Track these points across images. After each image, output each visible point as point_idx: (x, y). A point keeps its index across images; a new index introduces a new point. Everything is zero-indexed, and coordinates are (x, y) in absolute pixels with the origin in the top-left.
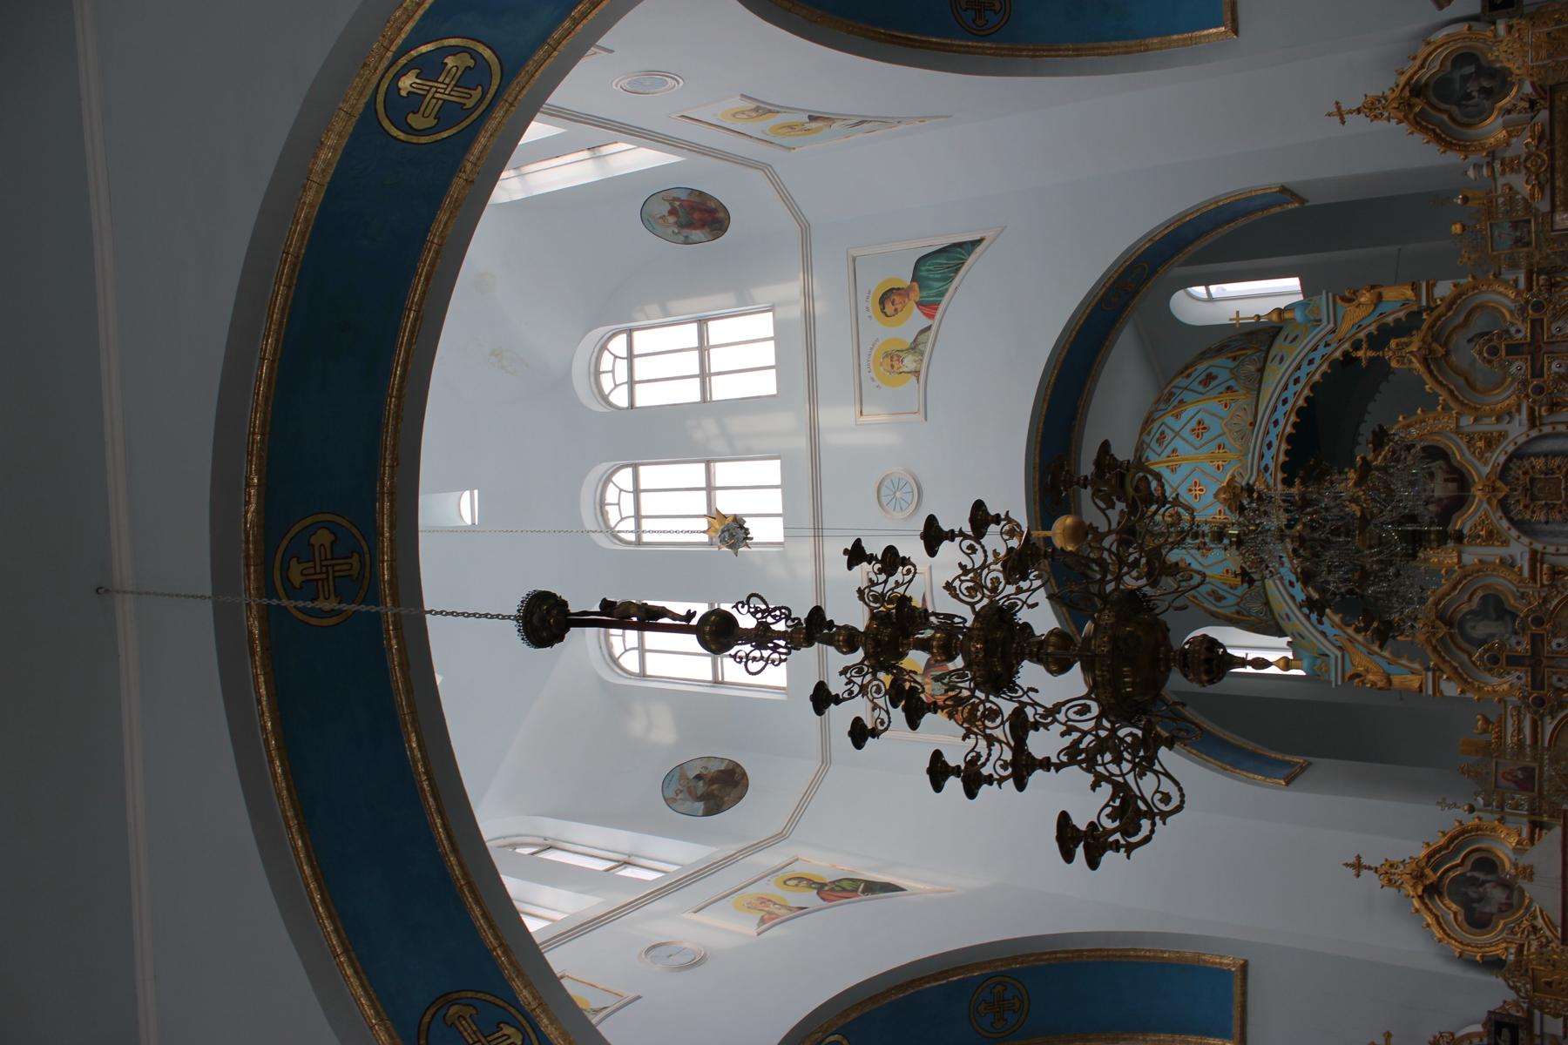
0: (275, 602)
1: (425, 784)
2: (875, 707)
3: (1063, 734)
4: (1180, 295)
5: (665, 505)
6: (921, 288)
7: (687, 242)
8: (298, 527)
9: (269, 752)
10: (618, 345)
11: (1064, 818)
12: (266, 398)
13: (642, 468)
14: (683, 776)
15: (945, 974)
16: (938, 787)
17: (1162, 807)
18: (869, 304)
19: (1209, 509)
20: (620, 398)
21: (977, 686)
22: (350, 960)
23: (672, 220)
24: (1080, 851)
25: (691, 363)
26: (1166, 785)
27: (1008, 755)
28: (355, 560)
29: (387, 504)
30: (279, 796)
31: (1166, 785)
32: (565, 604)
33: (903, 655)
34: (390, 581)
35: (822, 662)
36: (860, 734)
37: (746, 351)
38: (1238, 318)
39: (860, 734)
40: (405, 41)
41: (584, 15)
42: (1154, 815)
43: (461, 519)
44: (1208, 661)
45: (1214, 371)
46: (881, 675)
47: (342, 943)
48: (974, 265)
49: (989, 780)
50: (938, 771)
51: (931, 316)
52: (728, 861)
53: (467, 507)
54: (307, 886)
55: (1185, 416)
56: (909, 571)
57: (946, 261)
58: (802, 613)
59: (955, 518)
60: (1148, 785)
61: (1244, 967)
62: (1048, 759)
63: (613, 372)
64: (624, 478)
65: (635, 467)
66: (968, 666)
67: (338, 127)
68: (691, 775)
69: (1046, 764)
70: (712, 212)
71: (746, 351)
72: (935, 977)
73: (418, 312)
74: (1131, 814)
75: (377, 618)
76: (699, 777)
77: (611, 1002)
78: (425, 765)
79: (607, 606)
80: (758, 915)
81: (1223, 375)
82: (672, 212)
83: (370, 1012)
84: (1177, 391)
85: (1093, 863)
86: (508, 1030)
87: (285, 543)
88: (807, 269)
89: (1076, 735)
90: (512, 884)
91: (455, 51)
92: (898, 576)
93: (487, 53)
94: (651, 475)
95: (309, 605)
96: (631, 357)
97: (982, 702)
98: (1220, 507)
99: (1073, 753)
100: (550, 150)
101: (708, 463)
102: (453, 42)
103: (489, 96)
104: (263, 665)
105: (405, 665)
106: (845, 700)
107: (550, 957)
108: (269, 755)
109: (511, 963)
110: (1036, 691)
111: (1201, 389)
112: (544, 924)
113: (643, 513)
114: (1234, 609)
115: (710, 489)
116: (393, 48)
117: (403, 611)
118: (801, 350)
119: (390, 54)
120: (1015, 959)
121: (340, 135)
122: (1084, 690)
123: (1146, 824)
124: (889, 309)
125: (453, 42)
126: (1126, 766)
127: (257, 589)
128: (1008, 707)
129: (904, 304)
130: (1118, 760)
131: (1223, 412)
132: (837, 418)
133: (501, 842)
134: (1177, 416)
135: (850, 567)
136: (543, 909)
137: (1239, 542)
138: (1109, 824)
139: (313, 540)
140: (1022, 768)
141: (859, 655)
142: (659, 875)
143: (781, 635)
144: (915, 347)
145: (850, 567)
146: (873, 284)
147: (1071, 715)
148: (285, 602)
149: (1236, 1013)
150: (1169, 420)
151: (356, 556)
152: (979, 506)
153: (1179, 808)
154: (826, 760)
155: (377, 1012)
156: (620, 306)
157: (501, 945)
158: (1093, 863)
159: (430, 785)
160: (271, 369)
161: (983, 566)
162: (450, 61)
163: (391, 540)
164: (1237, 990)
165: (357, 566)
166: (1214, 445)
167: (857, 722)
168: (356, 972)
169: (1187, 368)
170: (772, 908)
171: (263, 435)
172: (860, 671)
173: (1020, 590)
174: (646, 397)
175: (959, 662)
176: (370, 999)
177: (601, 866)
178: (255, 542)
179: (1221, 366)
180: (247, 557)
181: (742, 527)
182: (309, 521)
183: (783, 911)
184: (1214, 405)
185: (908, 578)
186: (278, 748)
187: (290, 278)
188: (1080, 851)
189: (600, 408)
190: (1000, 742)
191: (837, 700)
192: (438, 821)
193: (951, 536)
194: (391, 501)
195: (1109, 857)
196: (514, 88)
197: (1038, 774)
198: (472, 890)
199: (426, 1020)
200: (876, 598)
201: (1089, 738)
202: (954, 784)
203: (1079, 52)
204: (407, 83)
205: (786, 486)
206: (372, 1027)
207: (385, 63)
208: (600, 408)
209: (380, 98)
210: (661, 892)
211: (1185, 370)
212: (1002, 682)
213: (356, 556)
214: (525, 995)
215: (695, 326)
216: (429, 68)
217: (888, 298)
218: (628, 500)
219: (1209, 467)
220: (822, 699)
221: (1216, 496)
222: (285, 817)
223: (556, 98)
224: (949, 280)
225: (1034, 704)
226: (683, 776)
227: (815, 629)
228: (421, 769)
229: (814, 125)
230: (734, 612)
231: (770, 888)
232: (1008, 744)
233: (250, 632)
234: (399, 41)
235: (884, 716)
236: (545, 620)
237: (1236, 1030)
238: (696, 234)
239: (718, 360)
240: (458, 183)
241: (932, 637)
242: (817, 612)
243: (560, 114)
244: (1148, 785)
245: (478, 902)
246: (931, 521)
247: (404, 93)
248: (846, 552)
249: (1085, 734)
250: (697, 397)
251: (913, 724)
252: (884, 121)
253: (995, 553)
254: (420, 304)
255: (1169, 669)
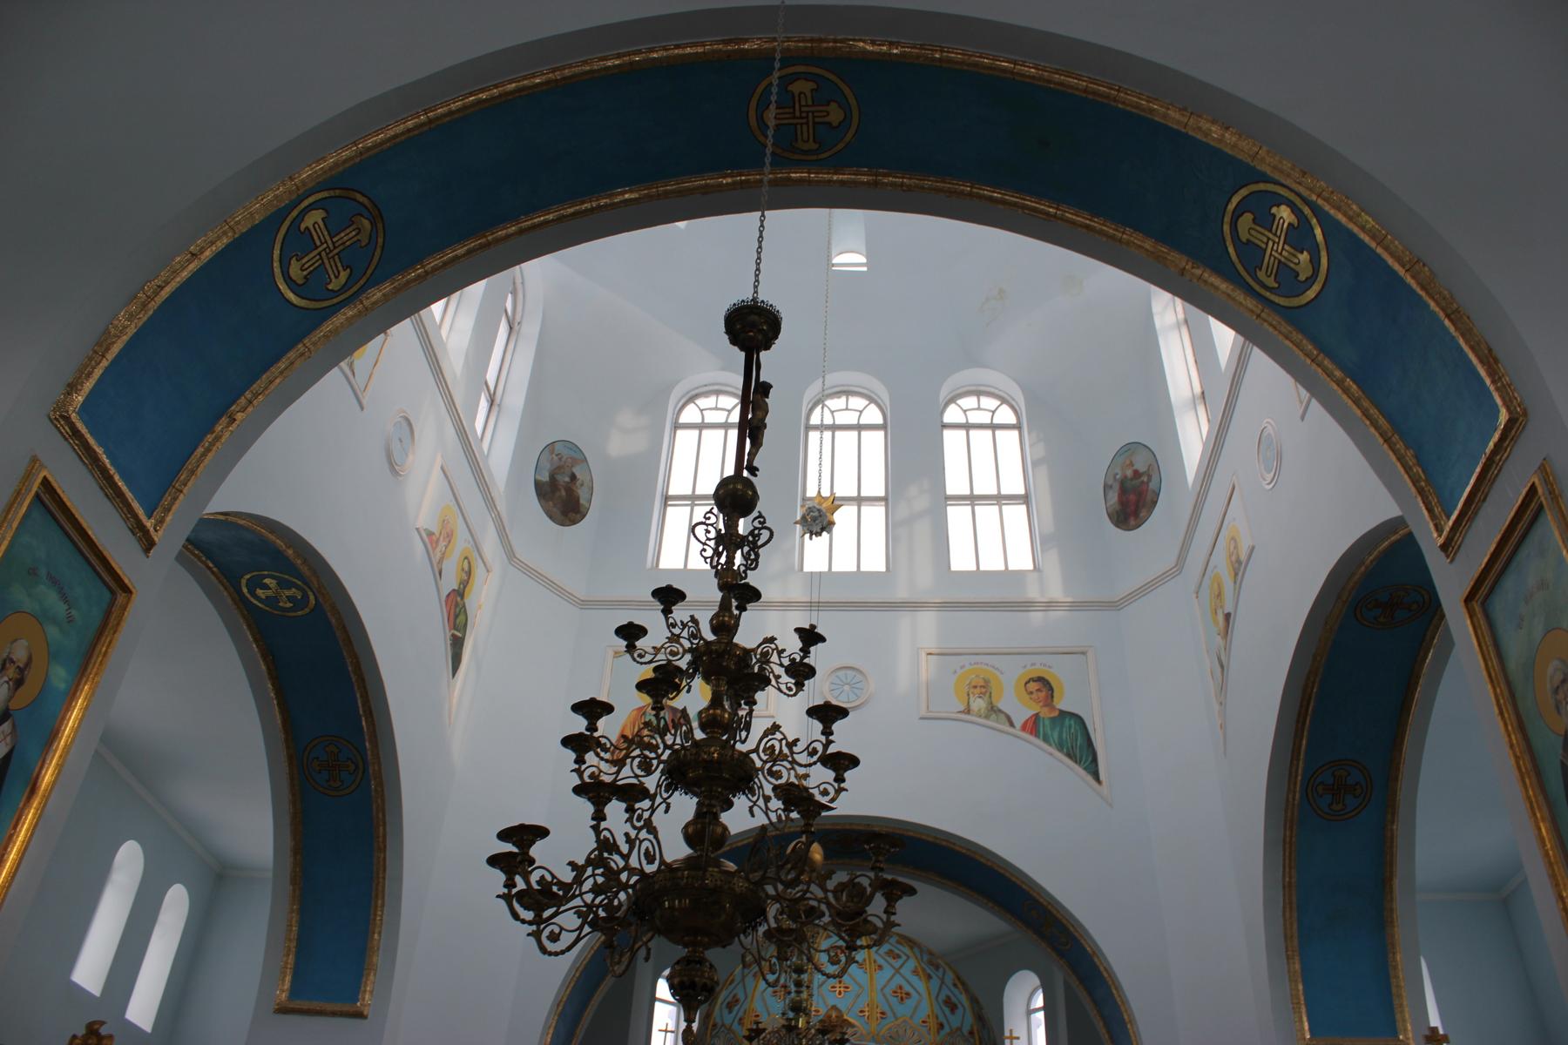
0: (777, 65)
1: (587, 205)
2: (657, 650)
3: (627, 835)
4: (1035, 980)
5: (842, 454)
6: (1053, 719)
7: (1107, 487)
8: (847, 91)
9: (628, 54)
10: (1006, 415)
11: (542, 832)
12: (976, 65)
13: (882, 433)
14: (575, 462)
15: (369, 713)
16: (578, 708)
17: (546, 933)
18: (1038, 666)
19: (826, 997)
20: (952, 414)
21: (675, 752)
22: (422, 125)
23: (1129, 473)
24: (509, 847)
25: (985, 486)
26: (567, 938)
27: (607, 779)
28: (813, 146)
29: (865, 179)
30: (585, 62)
31: (567, 938)
32: (767, 348)
33: (707, 679)
34: (790, 179)
35: (704, 604)
36: (631, 633)
37: (994, 540)
38: (1012, 1038)
39: (631, 633)
40: (1327, 214)
41: (1346, 391)
42: (538, 925)
43: (840, 250)
44: (693, 985)
45: (960, 1011)
46: (688, 657)
47: (437, 118)
48: (1074, 773)
49: (580, 760)
50: (592, 709)
51: (1024, 728)
52: (490, 502)
53: (850, 259)
54: (496, 86)
55: (915, 980)
56: (790, 689)
57: (1079, 745)
58: (753, 579)
59: (844, 737)
60: (569, 920)
61: (360, 1015)
62: (604, 819)
63: (979, 408)
64: (873, 415)
65: (883, 427)
66: (696, 744)
67: (1243, 144)
68: (577, 471)
69: (599, 816)
70: (1136, 514)
71: (994, 540)
72: (366, 702)
73: (1055, 216)
74: (539, 902)
75: (758, 164)
76: (573, 477)
77: (359, 381)
78: (606, 206)
79: (765, 389)
80: (436, 531)
81: (955, 1020)
82: (1137, 474)
83: (369, 143)
84: (940, 973)
85: (494, 861)
86: (344, 275)
87: (832, 77)
88: (1076, 606)
89: (625, 848)
90: (478, 289)
91: (1315, 262)
92: (785, 679)
93: (1311, 294)
94: (875, 443)
95: (774, 98)
96: (993, 427)
97: (658, 757)
98: (823, 1011)
99: (606, 845)
100: (1203, 351)
101: (885, 499)
102: (1324, 261)
103: (1268, 294)
104: (714, 52)
105: (706, 190)
106: (667, 619)
107: (406, 325)
108: (624, 55)
109: (408, 282)
110: (666, 811)
111: (942, 997)
112: (438, 318)
113: (838, 433)
114: (718, 1021)
115: (859, 500)
116: (1320, 202)
117: (765, 189)
118: (995, 596)
119: (1314, 198)
120: (380, 784)
121: (1235, 146)
122: (669, 859)
123: (528, 915)
124: (1033, 686)
125: (1324, 261)
126: (589, 898)
127: (788, 49)
128: (651, 783)
129: (1037, 701)
130: (596, 890)
131: (918, 1020)
132: (926, 629)
133: (518, 281)
134: (915, 972)
135: (798, 630)
136: (453, 318)
137: (790, 1028)
138: (534, 877)
139: (833, 106)
140: (595, 792)
141: (709, 636)
142: (479, 432)
143: (730, 560)
144: (993, 710)
145: (798, 630)
146: (1059, 671)
147: (646, 844)
148: (776, 75)
149: (315, 1005)
150: (912, 964)
151: (815, 146)
152: (853, 761)
153: (544, 950)
154: (585, 604)
155: (368, 149)
156: (1042, 418)
157: (427, 273)
158: (494, 861)
159: (586, 210)
160: (1005, 70)
161: (794, 762)
162: (1304, 257)
163: (830, 181)
164: (337, 1007)
165: (806, 147)
166: (886, 1009)
167: (641, 631)
168: (409, 130)
169: (963, 984)
170: (442, 544)
171: (940, 60)
172: (693, 636)
173: (767, 799)
174: (953, 441)
175: (699, 735)
176: (383, 143)
177: (491, 377)
178: (834, 49)
179: (963, 1019)
180: (821, 40)
181: (823, 529)
182: (853, 102)
183: (439, 555)
184: (925, 1010)
185: (783, 687)
186: (632, 63)
187: (1094, 93)
188: (509, 847)
189: (944, 393)
190: (618, 773)
191: (667, 612)
192: (551, 217)
193: (827, 732)
194: (868, 183)
195: (499, 877)
196: (1275, 319)
197: (589, 808)
198: (482, 247)
199: (359, 197)
200: (765, 655)
201: (621, 863)
202: (579, 725)
203: (1287, 887)
204: (1284, 214)
205: (859, 576)
206: (355, 143)
207: (1305, 193)
208: (944, 393)
209: (1262, 186)
210: (463, 434)
211: (960, 982)
212: (679, 775)
213: (815, 146)
214: (376, 294)
215: (1022, 492)
216: (1299, 236)
217: (1043, 686)
218: (851, 419)
219: (862, 1003)
220: (668, 597)
221: (834, 1007)
222: (564, 68)
223: (1259, 357)
224: (1060, 747)
225: (653, 809)
226: (575, 462)
227: (738, 593)
228: (602, 202)
229: (1221, 618)
230: (755, 514)
231: (461, 543)
232: (615, 780)
233: (746, 41)
234: (1327, 208)
235: (648, 658)
236: (752, 327)
237: (297, 1004)
238: (1114, 497)
239: (987, 513)
240: (1181, 260)
241: (724, 710)
242: (753, 595)
243: (1241, 362)
244: (569, 920)
245: (469, 252)
246: (842, 713)
247: (1274, 210)
248: (813, 627)
249: (626, 857)
250: (949, 491)
251: (642, 686)
252: (1222, 688)
253: (806, 776)
254: (1063, 219)
255: (685, 946)
